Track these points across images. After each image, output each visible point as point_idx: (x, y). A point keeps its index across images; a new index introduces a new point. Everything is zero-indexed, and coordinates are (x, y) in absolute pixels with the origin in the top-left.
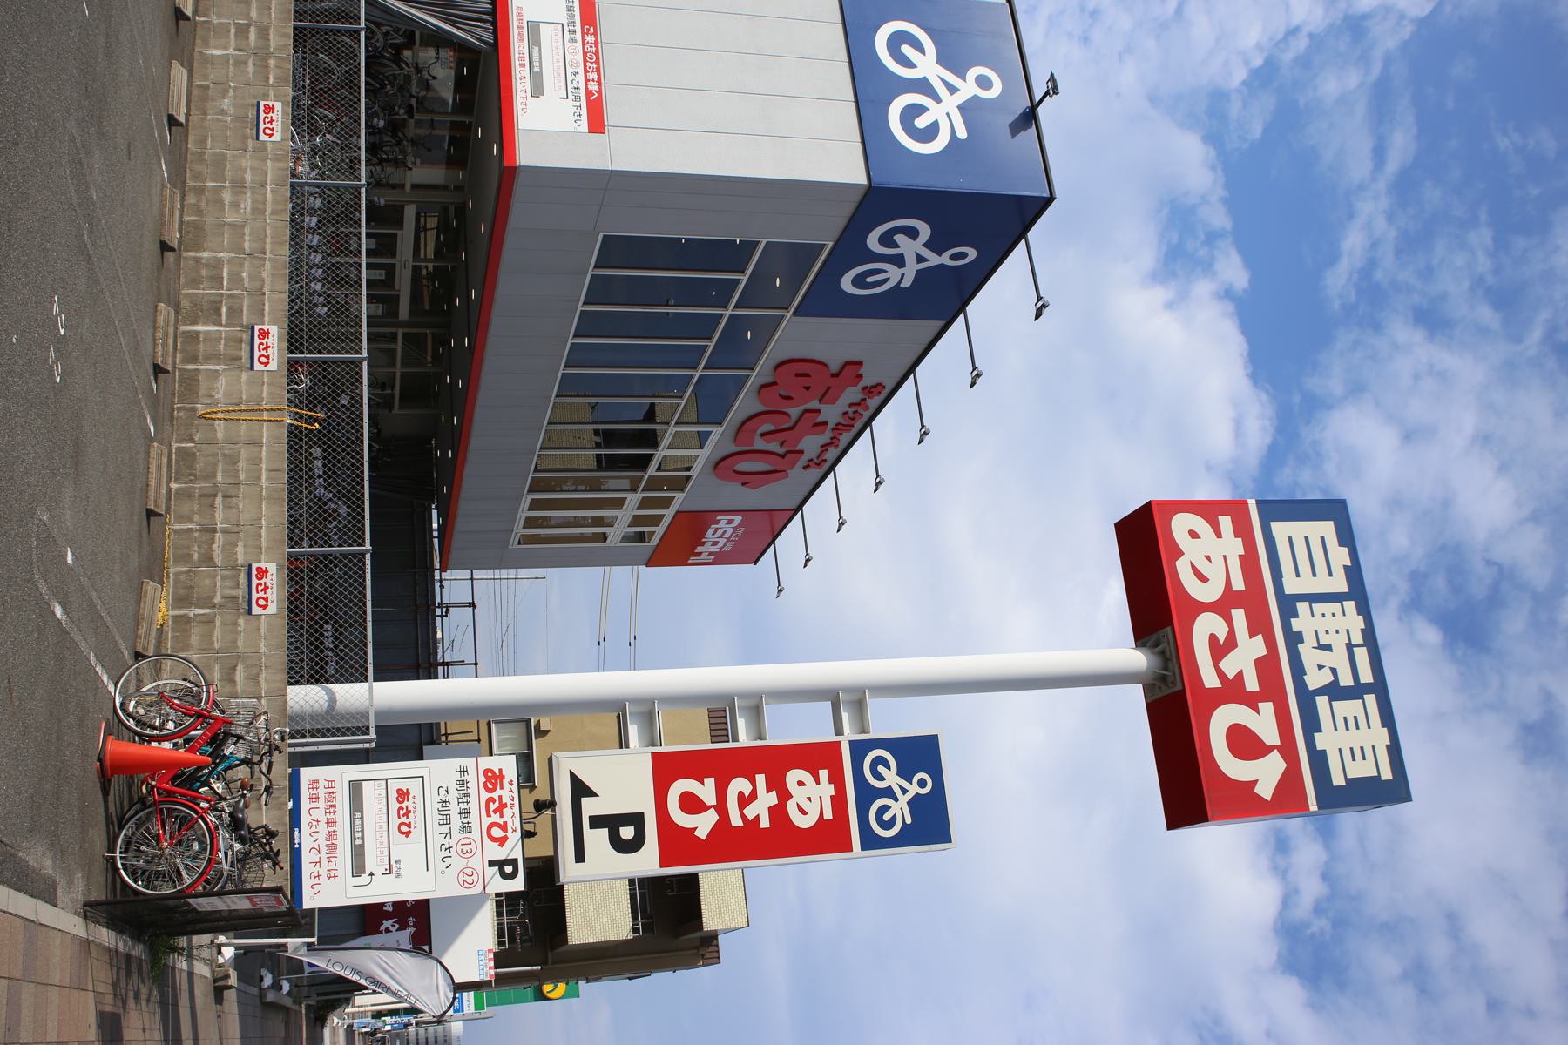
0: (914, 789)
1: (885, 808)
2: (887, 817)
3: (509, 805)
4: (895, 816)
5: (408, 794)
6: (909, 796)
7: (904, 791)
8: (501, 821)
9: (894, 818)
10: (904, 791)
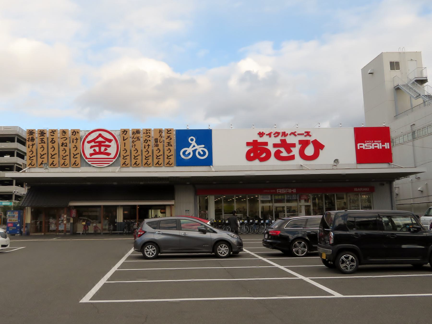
0: (194, 143)
1: (199, 153)
2: (202, 153)
3: (283, 138)
4: (202, 150)
5: (255, 143)
6: (196, 145)
7: (194, 146)
8: (298, 146)
9: (202, 151)
10: (194, 146)
